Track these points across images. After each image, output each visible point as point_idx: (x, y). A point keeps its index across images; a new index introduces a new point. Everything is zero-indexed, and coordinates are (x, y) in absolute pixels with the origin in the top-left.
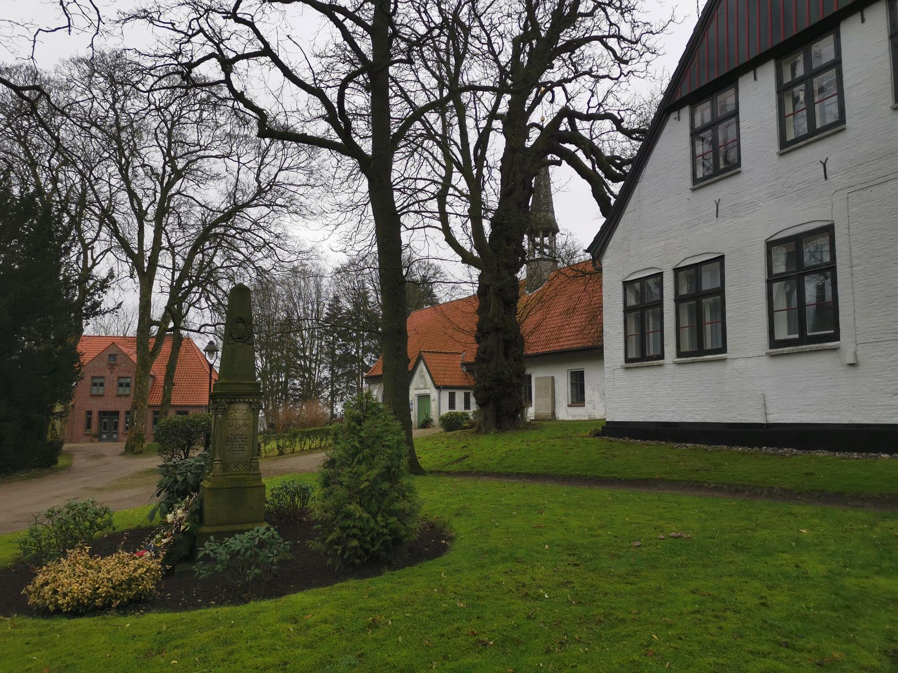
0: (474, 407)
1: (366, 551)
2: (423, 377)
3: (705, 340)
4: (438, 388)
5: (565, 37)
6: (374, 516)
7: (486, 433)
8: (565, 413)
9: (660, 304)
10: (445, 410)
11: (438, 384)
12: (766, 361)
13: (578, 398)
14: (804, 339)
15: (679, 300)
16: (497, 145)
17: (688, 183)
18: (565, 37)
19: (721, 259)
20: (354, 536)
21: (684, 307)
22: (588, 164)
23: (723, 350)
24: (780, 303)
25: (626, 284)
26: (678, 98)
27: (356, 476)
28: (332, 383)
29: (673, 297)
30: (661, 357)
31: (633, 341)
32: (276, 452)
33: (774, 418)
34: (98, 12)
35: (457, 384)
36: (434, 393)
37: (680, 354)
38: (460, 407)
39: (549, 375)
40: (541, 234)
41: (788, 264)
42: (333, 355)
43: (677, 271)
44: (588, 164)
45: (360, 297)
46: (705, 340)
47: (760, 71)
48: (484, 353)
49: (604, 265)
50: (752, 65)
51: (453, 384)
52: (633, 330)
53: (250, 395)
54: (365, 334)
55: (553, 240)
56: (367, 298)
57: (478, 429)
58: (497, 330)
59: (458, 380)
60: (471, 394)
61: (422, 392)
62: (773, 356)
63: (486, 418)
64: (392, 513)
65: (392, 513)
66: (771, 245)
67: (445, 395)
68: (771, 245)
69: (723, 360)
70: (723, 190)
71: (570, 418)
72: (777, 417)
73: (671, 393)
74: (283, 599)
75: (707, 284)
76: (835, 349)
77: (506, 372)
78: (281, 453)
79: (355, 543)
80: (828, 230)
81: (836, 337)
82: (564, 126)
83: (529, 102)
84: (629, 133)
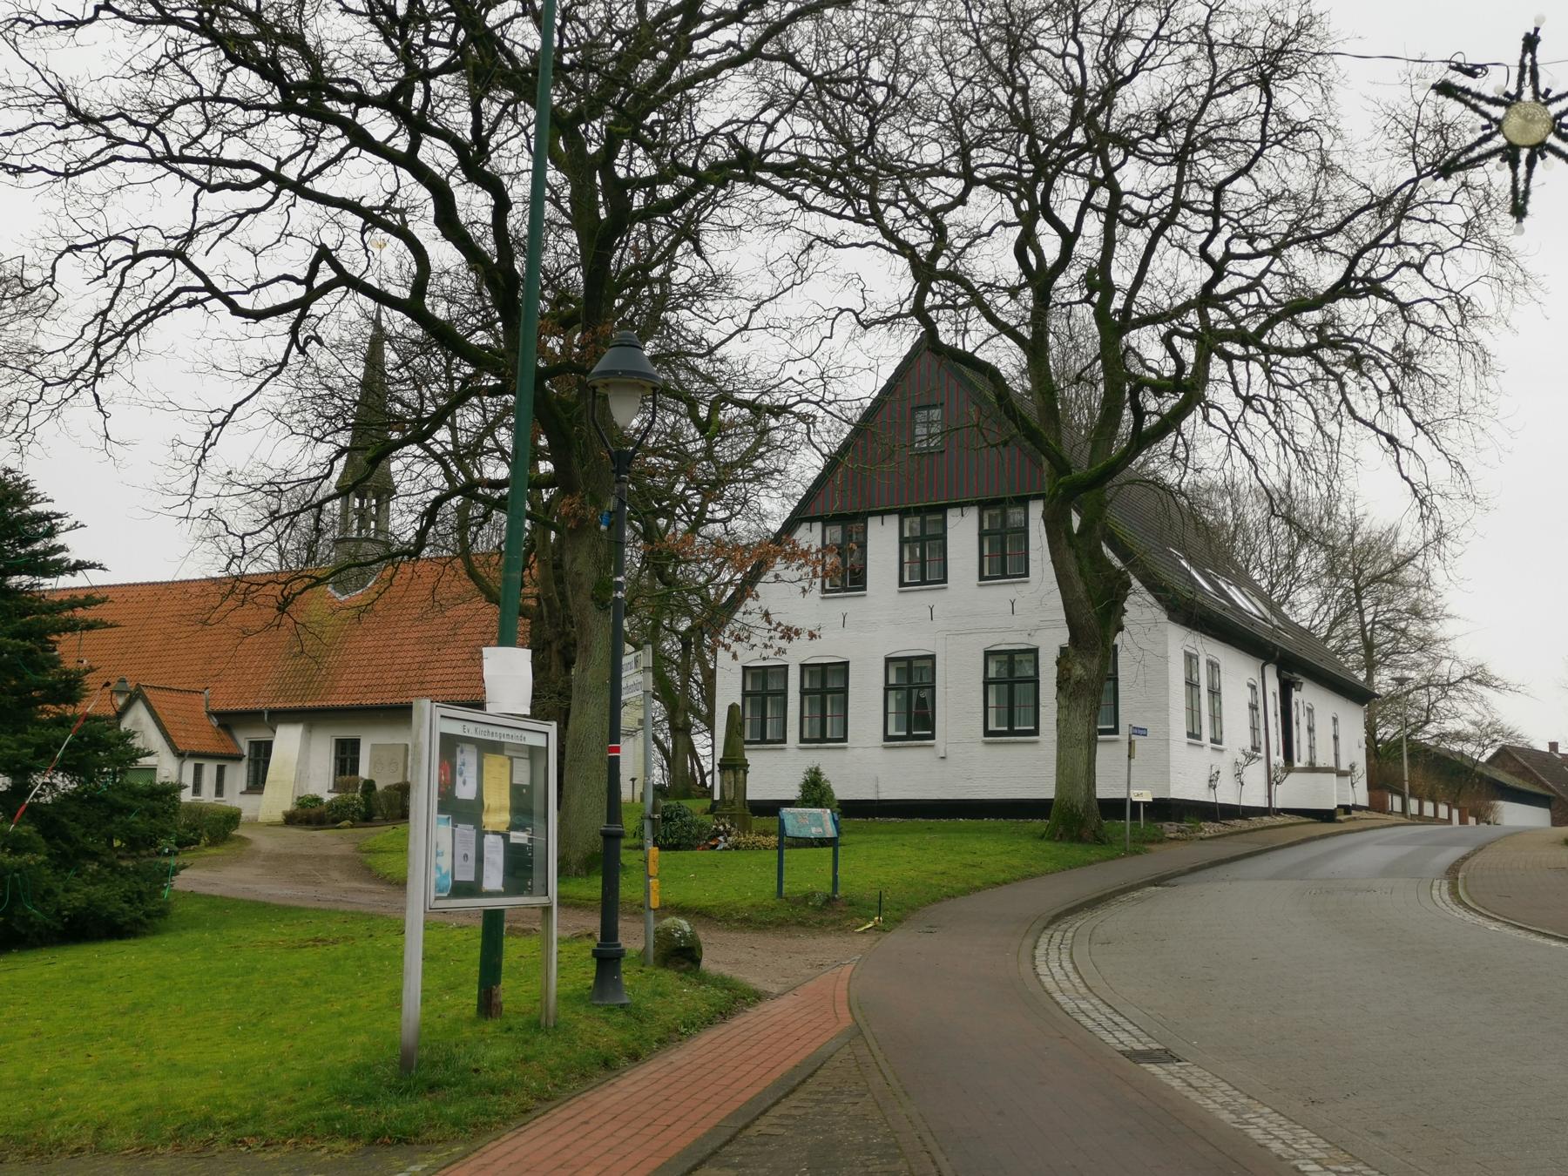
4: (180, 755)
11: (182, 748)
12: (881, 751)
15: (803, 692)
19: (846, 664)
23: (845, 740)
24: (892, 707)
29: (798, 688)
30: (784, 741)
33: (883, 796)
34: (240, 404)
35: (204, 750)
37: (802, 740)
41: (898, 677)
43: (803, 666)
62: (886, 747)
66: (889, 661)
67: (189, 767)
68: (889, 661)
72: (886, 795)
74: (736, 1022)
75: (833, 683)
76: (932, 746)
80: (932, 658)
81: (932, 737)
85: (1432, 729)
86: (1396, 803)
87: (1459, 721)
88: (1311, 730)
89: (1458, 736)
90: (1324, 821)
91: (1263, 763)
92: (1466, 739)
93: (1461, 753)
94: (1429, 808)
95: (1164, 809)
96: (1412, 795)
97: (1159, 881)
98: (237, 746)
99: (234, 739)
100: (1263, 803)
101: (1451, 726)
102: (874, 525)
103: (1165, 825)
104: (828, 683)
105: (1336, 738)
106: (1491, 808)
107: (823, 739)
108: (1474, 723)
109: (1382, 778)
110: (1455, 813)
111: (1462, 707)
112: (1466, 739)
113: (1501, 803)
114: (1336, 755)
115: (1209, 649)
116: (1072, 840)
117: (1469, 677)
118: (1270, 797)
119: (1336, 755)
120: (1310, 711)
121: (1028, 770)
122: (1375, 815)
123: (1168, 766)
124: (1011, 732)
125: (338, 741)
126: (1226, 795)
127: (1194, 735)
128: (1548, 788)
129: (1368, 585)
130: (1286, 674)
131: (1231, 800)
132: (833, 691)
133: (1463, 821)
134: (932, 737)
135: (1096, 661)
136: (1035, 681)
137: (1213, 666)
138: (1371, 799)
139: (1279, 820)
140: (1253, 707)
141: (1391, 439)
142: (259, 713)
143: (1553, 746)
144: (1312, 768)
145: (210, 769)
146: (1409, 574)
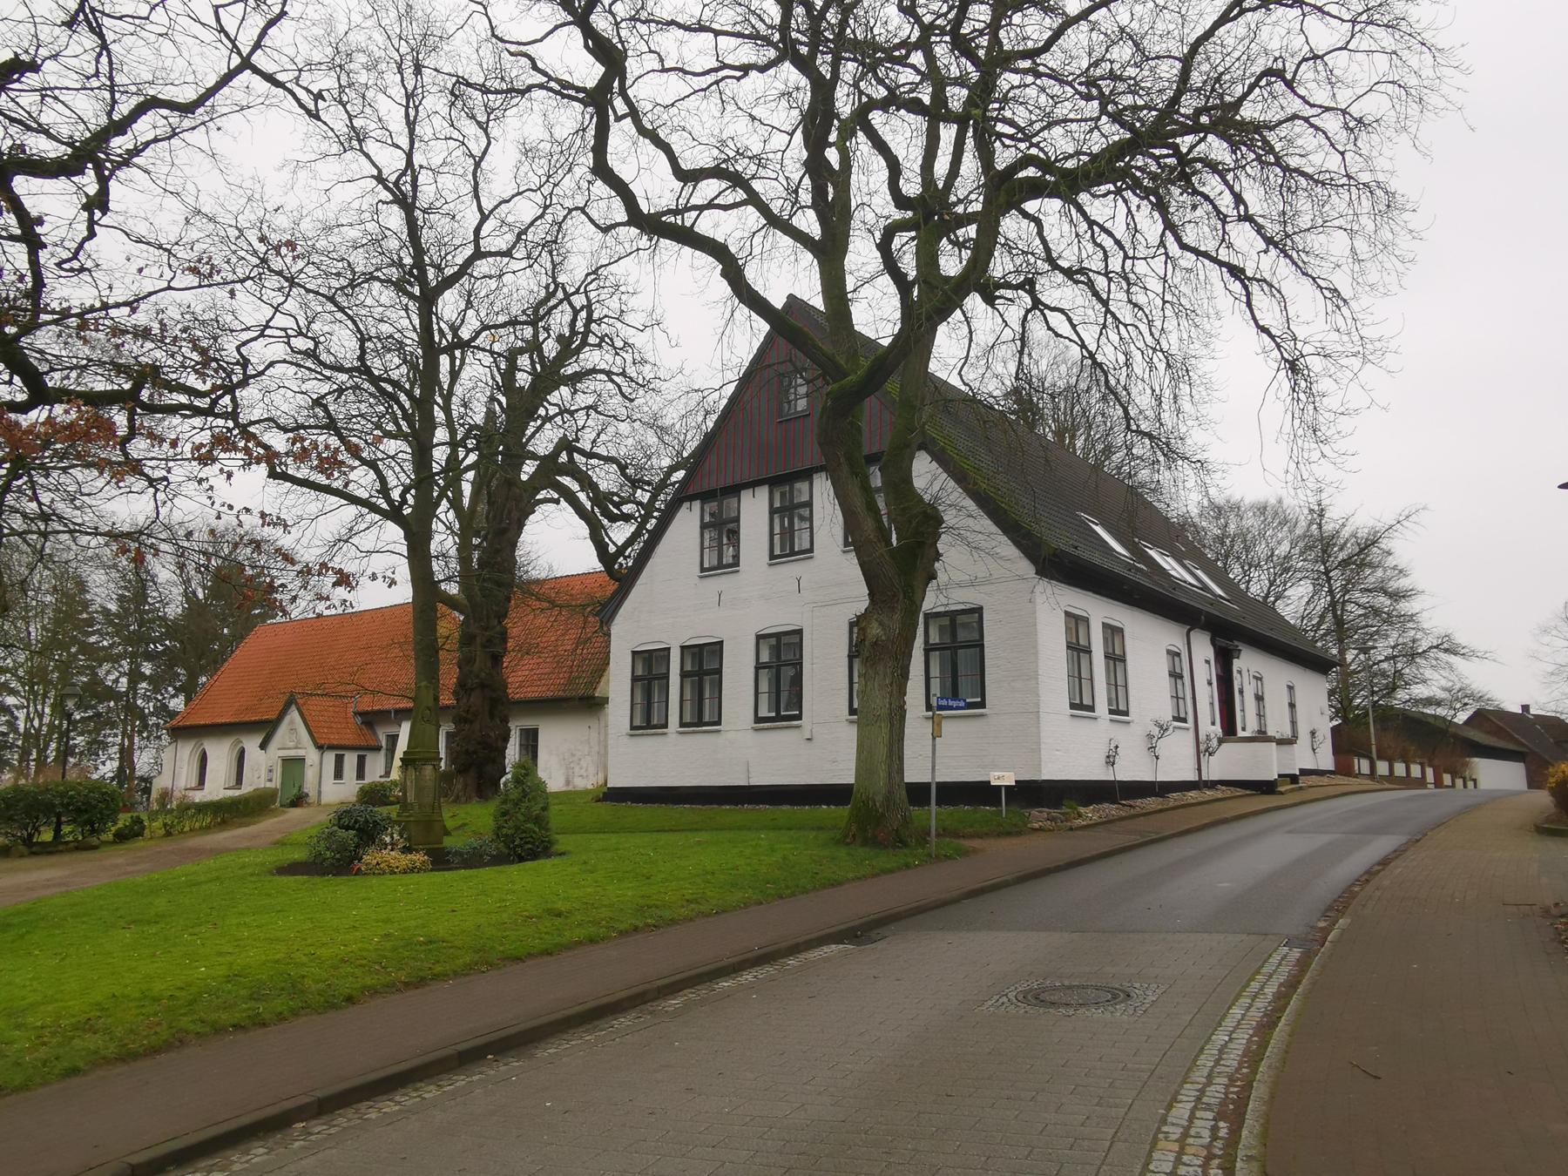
2: (293, 730)
3: (703, 715)
4: (320, 748)
9: (666, 677)
12: (751, 734)
14: (779, 718)
15: (684, 675)
21: (688, 682)
22: (588, 505)
25: (634, 653)
30: (666, 726)
31: (638, 708)
32: (163, 832)
33: (755, 781)
35: (347, 743)
36: (312, 755)
37: (682, 725)
43: (683, 648)
44: (588, 505)
46: (703, 715)
49: (613, 631)
50: (753, 485)
52: (638, 699)
61: (292, 753)
62: (756, 730)
66: (760, 638)
67: (330, 757)
68: (760, 638)
70: (722, 583)
73: (675, 759)
76: (798, 727)
78: (168, 834)
80: (799, 632)
81: (799, 717)
82: (564, 457)
83: (528, 433)
85: (1401, 695)
86: (1365, 766)
87: (1429, 685)
88: (1259, 698)
89: (1429, 701)
91: (1191, 733)
92: (1439, 703)
93: (1435, 716)
94: (1400, 769)
95: (1032, 793)
96: (1380, 758)
97: (858, 933)
98: (378, 740)
99: (375, 734)
100: (1191, 776)
101: (1420, 691)
102: (746, 496)
103: (1034, 812)
104: (704, 662)
105: (1292, 706)
106: (1466, 765)
107: (700, 723)
108: (1445, 689)
109: (1347, 742)
110: (1429, 771)
111: (1428, 673)
112: (1439, 703)
113: (1476, 760)
114: (1293, 723)
115: (1099, 611)
116: (865, 843)
117: (1437, 647)
118: (1199, 770)
119: (1293, 723)
121: (823, 749)
122: (1340, 779)
123: (1039, 744)
126: (1133, 769)
127: (1081, 706)
128: (1523, 745)
130: (1223, 642)
131: (1145, 775)
132: (709, 673)
133: (1438, 783)
134: (799, 717)
135: (897, 616)
138: (1337, 763)
140: (1176, 676)
141: (1236, 272)
142: (389, 712)
143: (1526, 708)
144: (1261, 737)
145: (350, 760)
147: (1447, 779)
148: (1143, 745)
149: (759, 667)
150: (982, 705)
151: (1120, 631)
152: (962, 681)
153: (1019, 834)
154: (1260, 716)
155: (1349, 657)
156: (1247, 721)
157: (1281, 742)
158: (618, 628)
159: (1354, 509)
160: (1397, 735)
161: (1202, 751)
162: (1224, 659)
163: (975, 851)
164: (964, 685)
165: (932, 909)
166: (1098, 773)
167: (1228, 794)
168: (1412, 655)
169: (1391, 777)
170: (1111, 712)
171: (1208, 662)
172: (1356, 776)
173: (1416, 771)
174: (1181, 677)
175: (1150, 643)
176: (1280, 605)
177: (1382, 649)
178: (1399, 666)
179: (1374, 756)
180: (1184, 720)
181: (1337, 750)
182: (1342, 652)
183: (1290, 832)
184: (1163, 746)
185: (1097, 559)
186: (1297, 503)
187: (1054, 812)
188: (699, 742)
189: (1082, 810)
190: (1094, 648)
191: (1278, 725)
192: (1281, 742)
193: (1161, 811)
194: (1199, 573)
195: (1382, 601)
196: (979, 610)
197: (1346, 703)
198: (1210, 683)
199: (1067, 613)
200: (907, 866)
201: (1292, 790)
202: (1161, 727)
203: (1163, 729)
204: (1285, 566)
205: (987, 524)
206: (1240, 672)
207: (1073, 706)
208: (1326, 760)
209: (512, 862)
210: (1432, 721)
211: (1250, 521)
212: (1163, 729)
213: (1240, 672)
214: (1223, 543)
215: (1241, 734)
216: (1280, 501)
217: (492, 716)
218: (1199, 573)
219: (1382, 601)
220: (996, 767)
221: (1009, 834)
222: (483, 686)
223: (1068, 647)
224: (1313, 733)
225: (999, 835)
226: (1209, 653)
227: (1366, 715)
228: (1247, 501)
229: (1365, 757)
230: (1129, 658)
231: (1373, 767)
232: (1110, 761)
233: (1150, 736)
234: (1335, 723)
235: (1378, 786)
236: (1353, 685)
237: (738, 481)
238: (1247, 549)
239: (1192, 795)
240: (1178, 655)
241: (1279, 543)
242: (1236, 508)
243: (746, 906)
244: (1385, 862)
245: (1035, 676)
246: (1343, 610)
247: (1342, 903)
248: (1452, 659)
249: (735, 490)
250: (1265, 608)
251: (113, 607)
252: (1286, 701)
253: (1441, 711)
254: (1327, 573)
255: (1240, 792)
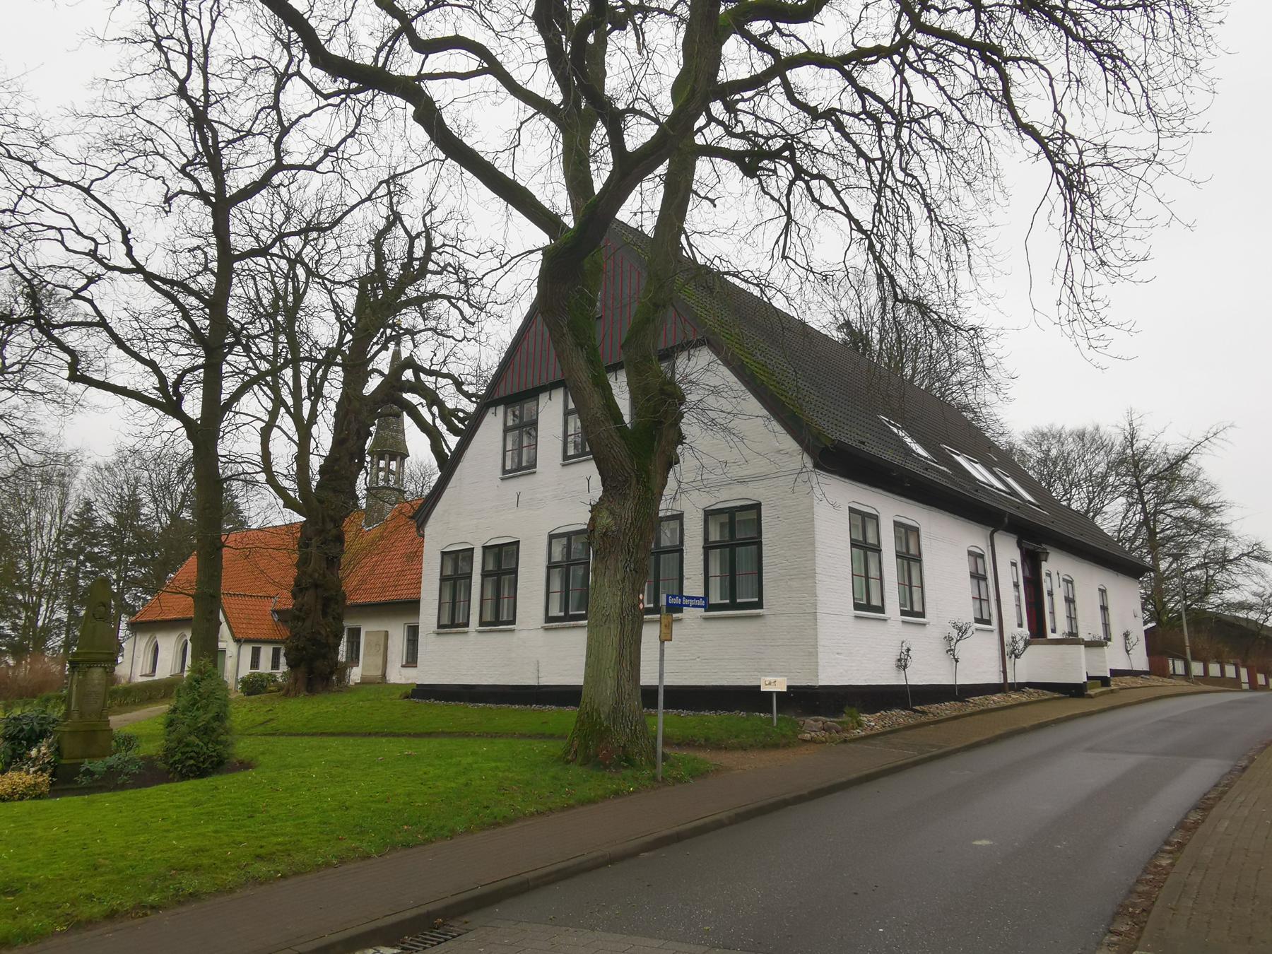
0: (283, 667)
1: (199, 768)
3: (500, 616)
4: (238, 641)
5: (411, 292)
6: (206, 744)
7: (296, 696)
8: (398, 675)
9: (469, 576)
10: (246, 670)
13: (412, 659)
15: (485, 575)
16: (334, 389)
17: (499, 473)
18: (411, 292)
20: (191, 758)
23: (513, 622)
25: (443, 554)
26: (496, 397)
27: (196, 718)
28: (69, 627)
29: (480, 571)
30: (467, 625)
31: (447, 608)
33: (545, 681)
35: (263, 637)
37: (482, 623)
38: (265, 666)
39: (383, 629)
40: (387, 456)
42: (75, 587)
43: (485, 548)
45: (128, 509)
46: (500, 616)
47: (554, 393)
48: (300, 610)
50: (550, 387)
51: (260, 636)
52: (447, 598)
53: (106, 661)
54: (131, 559)
55: (401, 465)
56: (138, 508)
57: (286, 692)
58: (316, 586)
59: (265, 631)
60: (282, 652)
62: (546, 629)
63: (296, 680)
64: (218, 743)
65: (218, 743)
66: (552, 537)
67: (247, 651)
68: (552, 537)
69: (512, 631)
71: (403, 681)
77: (323, 632)
79: (192, 762)
84: (468, 396)
85: (1214, 599)
86: (1179, 667)
87: (1241, 590)
88: (1070, 601)
89: (1242, 606)
90: (1072, 696)
91: (996, 636)
92: (1250, 607)
94: (1214, 670)
95: (809, 700)
96: (1195, 658)
100: (996, 679)
101: (1232, 596)
102: (543, 398)
103: (810, 721)
104: (503, 559)
105: (1104, 608)
108: (1255, 594)
109: (1161, 644)
110: (1244, 672)
111: (1240, 579)
114: (1106, 625)
115: (890, 510)
117: (1248, 555)
118: (1005, 672)
119: (1106, 625)
120: (1069, 582)
121: (546, 653)
122: (1155, 681)
123: (815, 646)
124: (734, 606)
125: (409, 627)
126: (918, 675)
127: (867, 606)
129: (1147, 482)
130: (1031, 546)
133: (1253, 686)
136: (679, 550)
137: (907, 533)
138: (1151, 663)
139: (1015, 697)
140: (978, 577)
144: (1072, 639)
146: (1185, 471)
147: (1261, 679)
148: (939, 648)
149: (551, 566)
150: (759, 605)
151: (916, 531)
152: (740, 580)
153: (787, 746)
154: (1072, 618)
155: (1163, 565)
156: (1058, 623)
157: (1090, 644)
158: (429, 530)
159: (1163, 435)
160: (1194, 633)
161: (1008, 652)
162: (1032, 561)
163: (718, 770)
164: (743, 584)
165: (547, 884)
166: (886, 676)
167: (1035, 697)
168: (1223, 562)
169: (1206, 679)
170: (903, 613)
171: (1014, 564)
172: (1171, 677)
173: (1230, 671)
174: (985, 578)
175: (948, 545)
176: (1098, 520)
177: (1195, 556)
178: (1211, 572)
179: (1189, 657)
180: (989, 622)
181: (1151, 651)
182: (1155, 559)
183: (1090, 749)
184: (962, 649)
185: (888, 455)
186: (1114, 432)
187: (831, 721)
188: (496, 641)
189: (864, 718)
190: (884, 547)
191: (1089, 627)
192: (1090, 644)
193: (956, 718)
194: (1010, 480)
195: (1194, 513)
196: (757, 507)
197: (1159, 607)
198: (1016, 585)
199: (851, 510)
200: (617, 794)
201: (1102, 694)
202: (960, 629)
203: (962, 631)
204: (1101, 485)
205: (753, 405)
206: (1049, 575)
207: (857, 607)
208: (1140, 660)
209: (172, 781)
210: (1244, 624)
211: (1070, 446)
212: (962, 631)
213: (1049, 575)
214: (1045, 465)
215: (1050, 636)
216: (1097, 429)
217: (325, 614)
218: (1010, 480)
219: (1194, 513)
220: (773, 672)
221: (776, 746)
222: (316, 586)
223: (853, 545)
224: (1126, 635)
225: (765, 747)
226: (1016, 556)
227: (1180, 617)
228: (1068, 429)
229: (1179, 658)
230: (925, 557)
231: (1187, 668)
232: (902, 664)
233: (949, 639)
234: (1150, 625)
235: (1194, 688)
236: (1167, 590)
237: (537, 384)
238: (1069, 471)
239: (997, 698)
240: (982, 556)
241: (1097, 465)
242: (1059, 437)
243: (342, 861)
244: (1204, 805)
245: (811, 575)
246: (1155, 521)
247: (1152, 877)
248: (1263, 565)
249: (533, 394)
250: (1085, 519)
251: (111, 521)
252: (1097, 603)
253: (1253, 615)
254: (1139, 485)
255: (1049, 695)
